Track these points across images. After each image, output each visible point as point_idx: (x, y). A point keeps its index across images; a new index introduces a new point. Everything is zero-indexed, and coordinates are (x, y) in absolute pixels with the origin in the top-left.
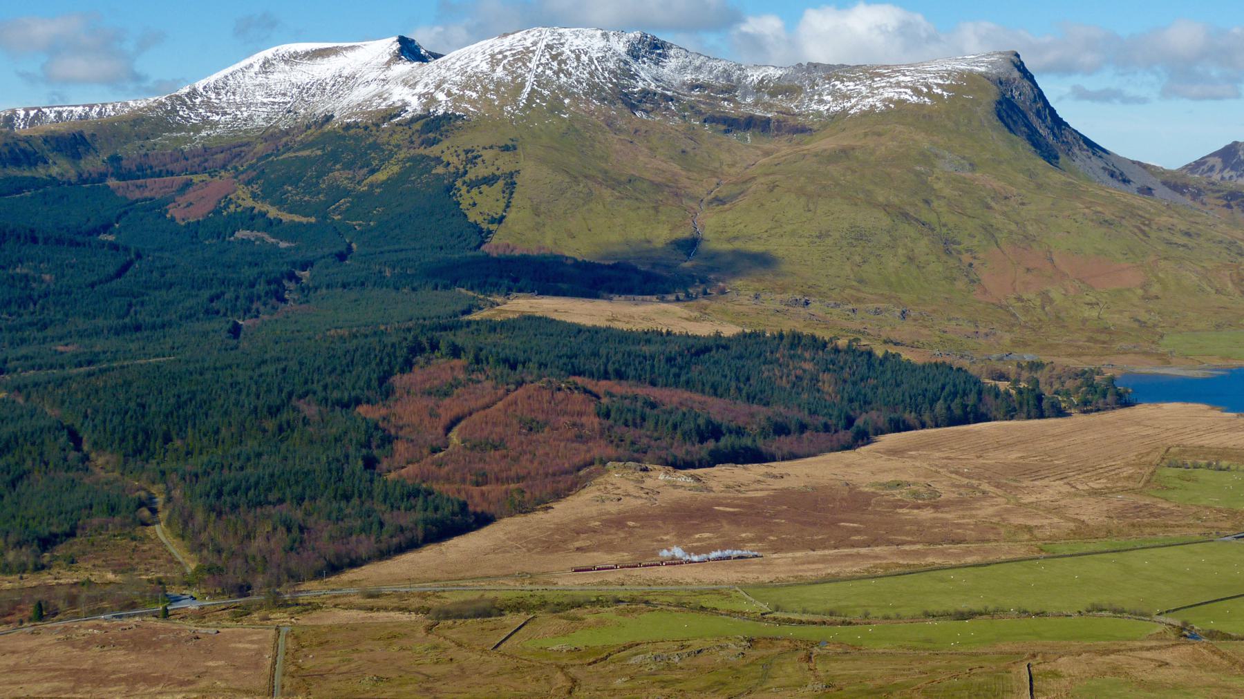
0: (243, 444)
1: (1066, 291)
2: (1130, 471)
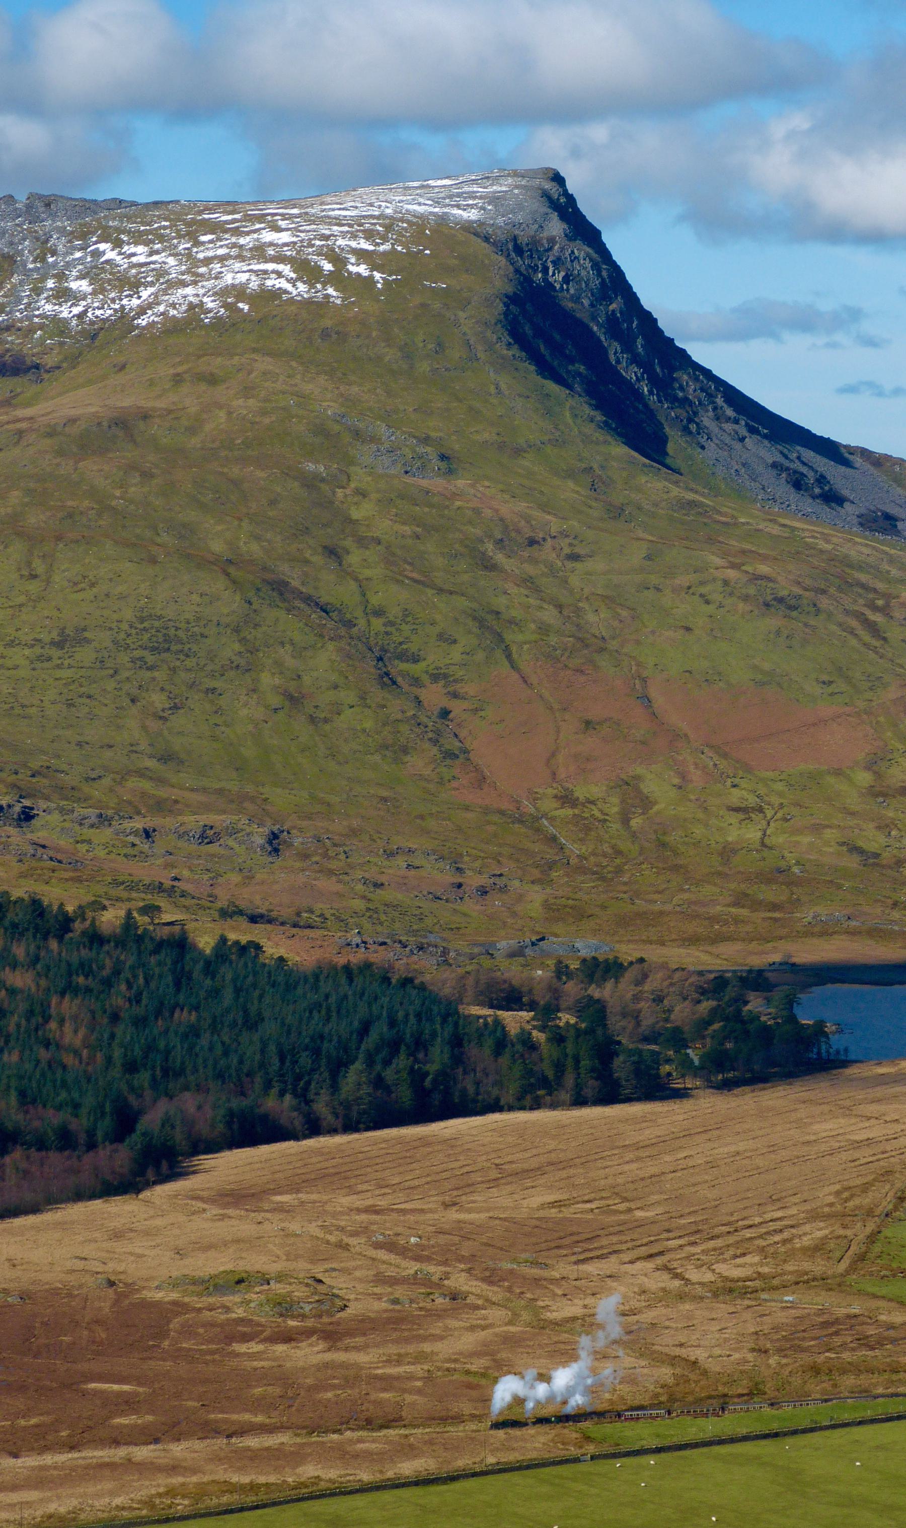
0: (783, 864)
1: (683, 776)
2: (817, 1232)
